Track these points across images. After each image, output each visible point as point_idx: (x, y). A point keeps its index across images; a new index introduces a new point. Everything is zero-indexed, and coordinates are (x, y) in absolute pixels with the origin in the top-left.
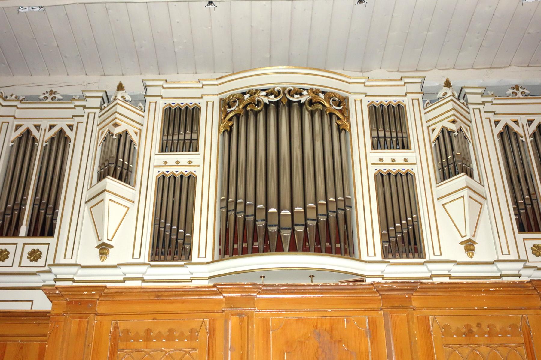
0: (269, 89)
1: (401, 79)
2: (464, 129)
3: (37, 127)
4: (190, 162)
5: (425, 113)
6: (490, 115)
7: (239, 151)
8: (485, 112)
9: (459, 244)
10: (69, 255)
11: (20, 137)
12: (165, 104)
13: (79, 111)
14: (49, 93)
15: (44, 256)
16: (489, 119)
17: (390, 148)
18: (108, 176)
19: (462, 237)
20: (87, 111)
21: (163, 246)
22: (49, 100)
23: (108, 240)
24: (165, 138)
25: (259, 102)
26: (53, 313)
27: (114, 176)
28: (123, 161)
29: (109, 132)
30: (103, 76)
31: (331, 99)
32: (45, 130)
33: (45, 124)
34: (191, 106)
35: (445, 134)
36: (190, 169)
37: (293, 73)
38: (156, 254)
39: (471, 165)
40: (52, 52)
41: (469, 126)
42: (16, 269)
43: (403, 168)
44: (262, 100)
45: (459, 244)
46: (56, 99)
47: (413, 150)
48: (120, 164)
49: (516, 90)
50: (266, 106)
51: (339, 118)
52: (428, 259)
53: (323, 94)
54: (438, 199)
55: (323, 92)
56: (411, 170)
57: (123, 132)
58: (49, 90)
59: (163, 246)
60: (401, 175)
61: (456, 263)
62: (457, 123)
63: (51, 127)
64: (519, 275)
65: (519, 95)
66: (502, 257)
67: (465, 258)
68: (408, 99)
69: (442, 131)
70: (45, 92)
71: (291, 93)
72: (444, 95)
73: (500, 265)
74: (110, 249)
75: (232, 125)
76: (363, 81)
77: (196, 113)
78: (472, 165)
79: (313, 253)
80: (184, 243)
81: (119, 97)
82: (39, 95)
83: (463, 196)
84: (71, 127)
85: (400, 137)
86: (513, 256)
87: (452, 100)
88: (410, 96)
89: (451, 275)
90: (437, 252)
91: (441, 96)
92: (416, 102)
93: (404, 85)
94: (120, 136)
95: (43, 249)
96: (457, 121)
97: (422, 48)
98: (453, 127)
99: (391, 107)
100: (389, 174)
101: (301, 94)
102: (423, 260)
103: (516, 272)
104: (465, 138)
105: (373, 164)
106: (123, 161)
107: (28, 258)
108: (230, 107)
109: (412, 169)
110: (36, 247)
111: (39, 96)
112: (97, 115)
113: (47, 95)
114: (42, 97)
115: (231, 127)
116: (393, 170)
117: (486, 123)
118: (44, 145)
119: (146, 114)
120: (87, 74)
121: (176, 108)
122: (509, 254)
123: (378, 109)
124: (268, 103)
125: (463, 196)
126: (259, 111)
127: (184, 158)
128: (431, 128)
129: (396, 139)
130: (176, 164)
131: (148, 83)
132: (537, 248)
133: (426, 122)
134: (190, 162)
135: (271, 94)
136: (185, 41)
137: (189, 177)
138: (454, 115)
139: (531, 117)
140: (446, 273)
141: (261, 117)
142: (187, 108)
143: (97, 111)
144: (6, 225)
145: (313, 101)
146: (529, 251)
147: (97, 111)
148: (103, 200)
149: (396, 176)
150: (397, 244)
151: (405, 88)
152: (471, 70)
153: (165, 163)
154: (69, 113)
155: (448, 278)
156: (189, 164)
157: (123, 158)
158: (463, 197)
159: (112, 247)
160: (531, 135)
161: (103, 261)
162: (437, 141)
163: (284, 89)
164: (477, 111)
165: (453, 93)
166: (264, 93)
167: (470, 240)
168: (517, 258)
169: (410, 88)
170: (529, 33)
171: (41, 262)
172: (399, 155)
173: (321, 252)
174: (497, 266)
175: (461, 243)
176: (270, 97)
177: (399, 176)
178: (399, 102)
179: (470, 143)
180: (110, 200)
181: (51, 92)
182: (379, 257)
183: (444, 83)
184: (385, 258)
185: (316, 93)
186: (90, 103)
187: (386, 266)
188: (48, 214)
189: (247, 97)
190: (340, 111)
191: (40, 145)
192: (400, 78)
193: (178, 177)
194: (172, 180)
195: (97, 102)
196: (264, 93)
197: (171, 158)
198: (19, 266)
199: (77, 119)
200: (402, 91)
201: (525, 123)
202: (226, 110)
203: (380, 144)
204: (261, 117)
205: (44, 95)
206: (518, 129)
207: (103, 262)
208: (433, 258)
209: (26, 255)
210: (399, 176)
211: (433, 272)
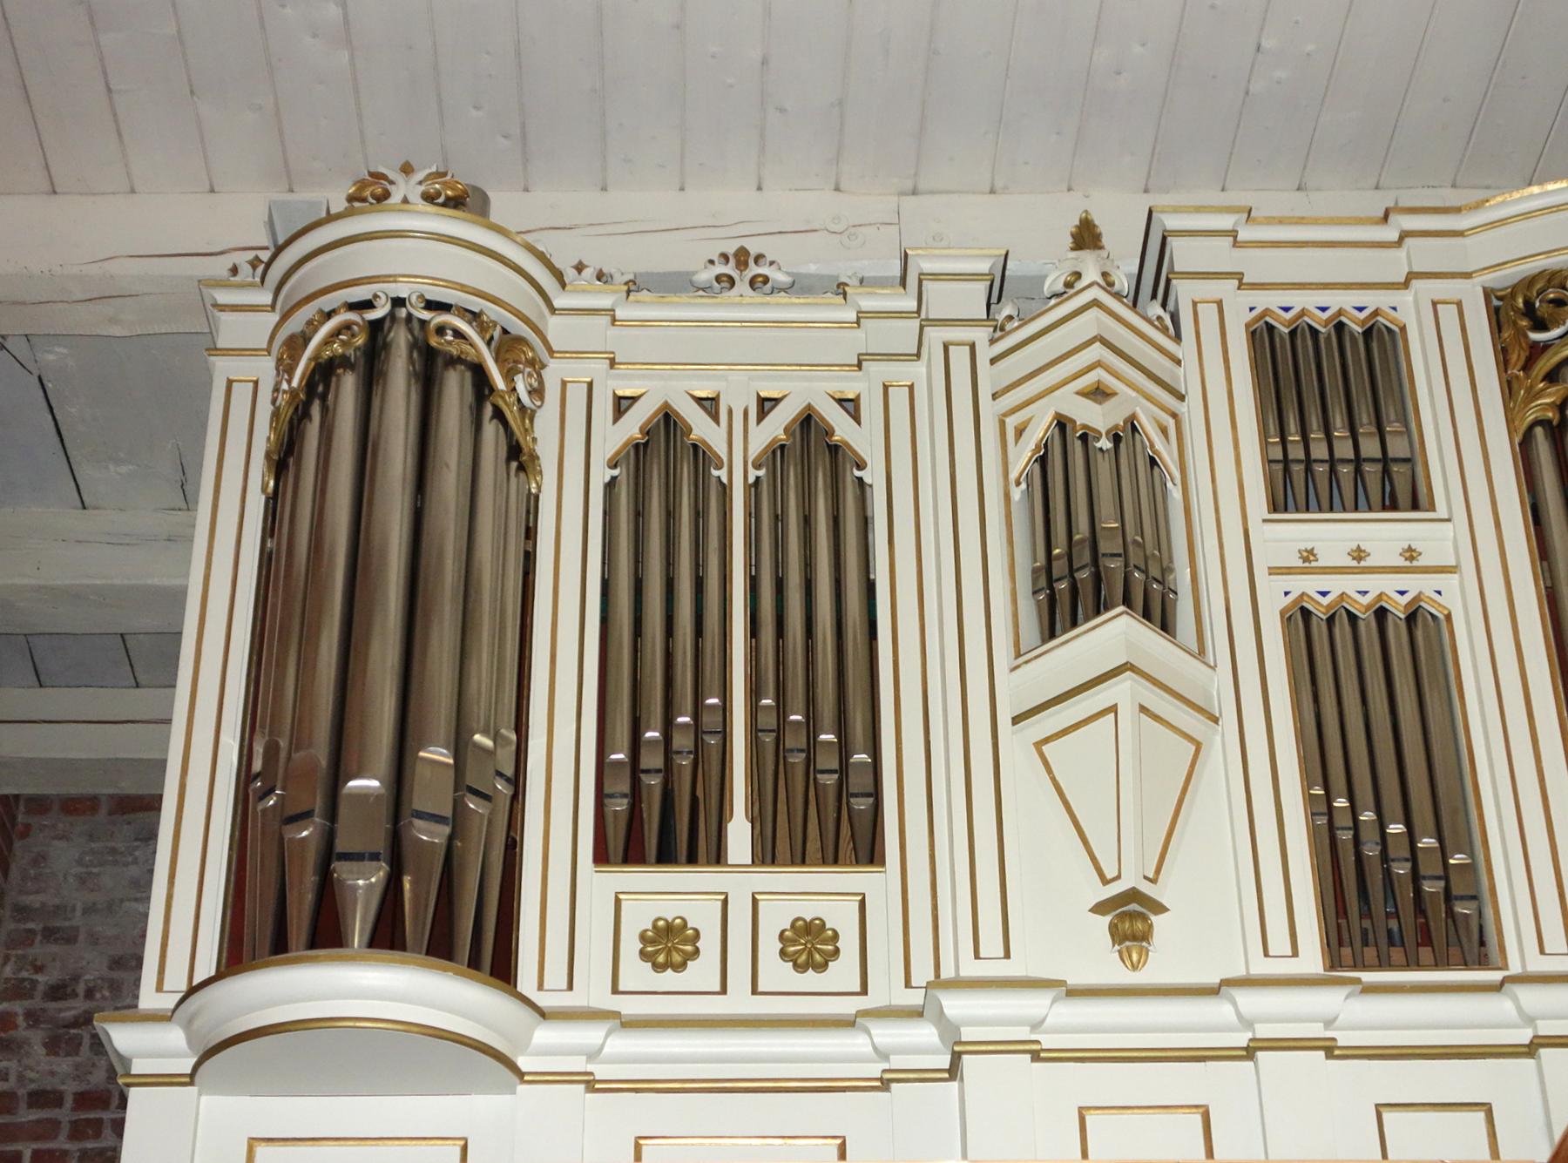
1: (1386, 218)
4: (1410, 553)
5: (993, 361)
7: (1073, 507)
11: (637, 446)
12: (1251, 309)
14: (732, 262)
17: (1304, 508)
20: (935, 336)
21: (1366, 913)
24: (1277, 453)
38: (1340, 944)
39: (1171, 577)
40: (731, 86)
41: (1174, 415)
42: (739, 1002)
43: (1396, 590)
46: (769, 285)
47: (1442, 512)
52: (1515, 968)
54: (1016, 720)
56: (1436, 597)
58: (731, 249)
59: (1366, 913)
60: (1353, 618)
61: (1361, 986)
63: (765, 405)
68: (1416, 302)
70: (715, 258)
72: (1069, 285)
73: (1250, 1001)
74: (1154, 918)
76: (1225, 222)
77: (1383, 351)
78: (1175, 579)
79: (423, 956)
80: (1448, 896)
81: (1091, 274)
82: (691, 269)
83: (1116, 705)
84: (624, 403)
85: (1348, 461)
89: (1334, 1039)
90: (991, 941)
91: (1059, 287)
92: (1448, 314)
93: (1399, 243)
98: (1097, 417)
99: (1303, 329)
100: (1381, 614)
102: (1495, 976)
105: (1274, 571)
108: (1541, 326)
111: (694, 273)
112: (985, 353)
113: (729, 269)
114: (706, 276)
118: (751, 480)
119: (1186, 350)
120: (842, 186)
121: (1256, 330)
123: (1328, 338)
125: (1116, 705)
128: (1011, 422)
129: (1379, 467)
132: (660, 943)
133: (995, 396)
134: (1410, 553)
136: (1310, 47)
137: (1412, 618)
138: (1098, 364)
140: (1316, 1031)
143: (981, 335)
144: (650, 815)
149: (1331, 621)
150: (1369, 909)
151: (1401, 254)
153: (1309, 555)
155: (1322, 1054)
156: (1407, 564)
158: (1113, 709)
161: (1135, 967)
165: (1105, 275)
167: (1133, 895)
173: (403, 948)
174: (1516, 1001)
175: (1100, 908)
178: (1340, 312)
179: (1175, 484)
181: (742, 258)
182: (1312, 959)
183: (1073, 235)
184: (1332, 967)
186: (941, 299)
187: (1347, 998)
188: (647, 771)
191: (738, 476)
192: (1381, 214)
193: (1320, 613)
194: (1342, 630)
195: (972, 299)
200: (1394, 265)
202: (1526, 336)
203: (1291, 482)
205: (720, 269)
206: (702, 428)
207: (1137, 974)
208: (1538, 965)
209: (770, 946)
211: (1257, 1026)
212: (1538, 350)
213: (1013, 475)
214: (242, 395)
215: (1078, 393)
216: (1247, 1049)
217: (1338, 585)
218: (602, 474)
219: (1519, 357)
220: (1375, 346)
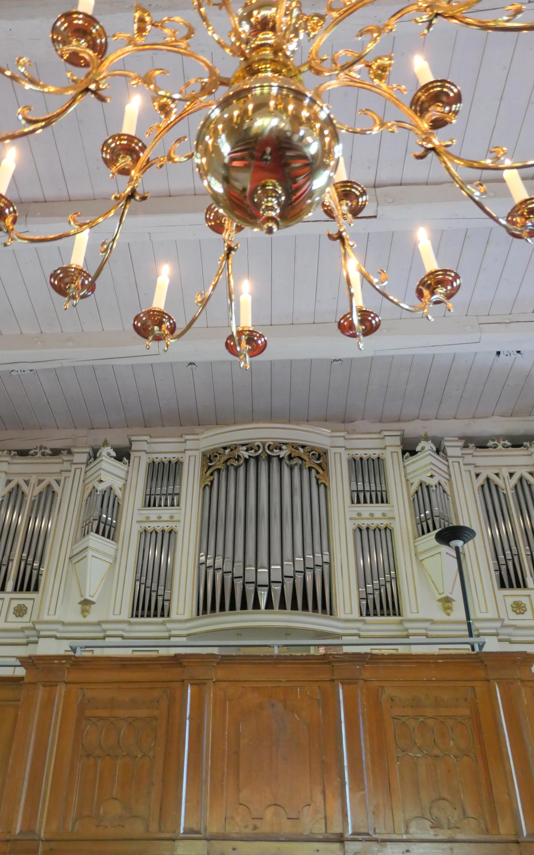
0: (249, 444)
1: (380, 433)
2: (443, 483)
3: (27, 482)
6: (471, 468)
8: (464, 464)
9: (437, 601)
10: (52, 612)
13: (66, 466)
15: (29, 611)
16: (470, 472)
18: (92, 533)
19: (440, 594)
20: (74, 466)
22: (39, 455)
23: (90, 596)
25: (239, 456)
26: (26, 681)
27: (97, 532)
28: (112, 521)
29: (94, 488)
30: (91, 429)
31: (311, 454)
32: (34, 485)
33: (33, 480)
34: (174, 461)
35: (423, 488)
36: (171, 525)
44: (243, 455)
45: (437, 601)
49: (497, 442)
50: (247, 461)
51: (318, 472)
53: (302, 448)
57: (107, 488)
58: (39, 445)
62: (434, 478)
64: (497, 634)
65: (500, 446)
69: (421, 485)
71: (271, 448)
75: (214, 479)
86: (490, 616)
87: (430, 454)
95: (28, 604)
96: (435, 476)
97: (402, 400)
98: (433, 482)
101: (281, 449)
103: (494, 631)
104: (444, 491)
105: (351, 519)
106: (112, 521)
107: (14, 613)
108: (211, 462)
109: (391, 524)
110: (21, 602)
115: (212, 482)
116: (371, 525)
117: (465, 475)
118: (33, 499)
120: (76, 427)
122: (487, 612)
124: (247, 457)
126: (239, 466)
127: (165, 513)
130: (158, 520)
131: (133, 438)
135: (252, 449)
139: (512, 471)
141: (242, 471)
142: (170, 462)
143: (83, 467)
145: (292, 456)
146: (509, 609)
147: (83, 467)
148: (85, 557)
152: (454, 420)
159: (93, 603)
160: (512, 488)
162: (416, 495)
163: (264, 444)
164: (456, 465)
166: (245, 448)
168: (497, 617)
169: (389, 441)
170: (508, 385)
171: (26, 618)
172: (378, 509)
175: (439, 600)
176: (250, 451)
180: (93, 556)
182: (356, 614)
185: (295, 447)
189: (227, 451)
190: (319, 465)
197: (153, 513)
199: (64, 474)
200: (181, 447)
201: (507, 475)
204: (242, 471)
206: (499, 482)
209: (12, 610)
210: (377, 531)
212: (210, 467)
213: (84, 500)
214: (192, 459)
215: (527, 472)
216: (407, 635)
217: (153, 525)
219: (205, 469)
220: (177, 466)
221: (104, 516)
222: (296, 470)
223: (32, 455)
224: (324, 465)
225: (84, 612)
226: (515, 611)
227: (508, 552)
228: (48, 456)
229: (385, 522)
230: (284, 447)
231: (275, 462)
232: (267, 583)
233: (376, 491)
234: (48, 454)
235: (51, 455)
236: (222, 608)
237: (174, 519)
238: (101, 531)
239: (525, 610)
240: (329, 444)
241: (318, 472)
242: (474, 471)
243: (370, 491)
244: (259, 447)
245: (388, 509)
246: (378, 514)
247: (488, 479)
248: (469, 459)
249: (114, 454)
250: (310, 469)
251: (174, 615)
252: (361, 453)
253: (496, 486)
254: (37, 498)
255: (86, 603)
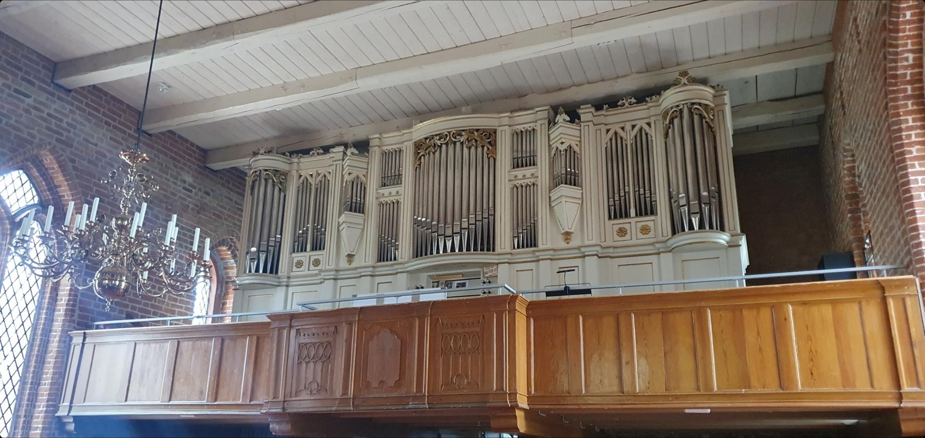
3: (623, 128)
22: (316, 155)
27: (566, 183)
33: (628, 127)
36: (396, 198)
37: (444, 121)
42: (634, 242)
48: (354, 201)
51: (488, 149)
55: (685, 84)
65: (627, 104)
66: (587, 243)
67: (563, 245)
86: (594, 242)
88: (539, 122)
94: (566, 150)
101: (462, 136)
106: (356, 199)
139: (634, 123)
154: (643, 114)
157: (356, 197)
163: (449, 133)
171: (652, 234)
177: (528, 186)
185: (471, 132)
190: (489, 143)
196: (438, 138)
198: (309, 270)
201: (630, 128)
209: (639, 230)
218: (604, 146)
221: (569, 170)
222: (473, 149)
223: (621, 106)
224: (493, 143)
225: (350, 262)
226: (642, 233)
227: (622, 191)
228: (635, 105)
229: (532, 180)
230: (463, 133)
231: (458, 144)
232: (451, 235)
233: (530, 156)
234: (634, 103)
235: (636, 103)
236: (421, 256)
237: (518, 178)
238: (568, 182)
239: (625, 234)
240: (497, 124)
241: (488, 149)
242: (604, 128)
243: (526, 157)
244: (446, 135)
245: (535, 170)
246: (528, 175)
247: (616, 133)
248: (602, 120)
249: (568, 119)
250: (483, 147)
251: (541, 246)
252: (520, 128)
253: (621, 138)
254: (634, 141)
255: (567, 235)
